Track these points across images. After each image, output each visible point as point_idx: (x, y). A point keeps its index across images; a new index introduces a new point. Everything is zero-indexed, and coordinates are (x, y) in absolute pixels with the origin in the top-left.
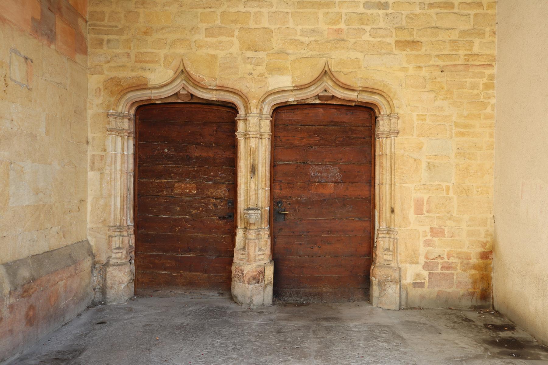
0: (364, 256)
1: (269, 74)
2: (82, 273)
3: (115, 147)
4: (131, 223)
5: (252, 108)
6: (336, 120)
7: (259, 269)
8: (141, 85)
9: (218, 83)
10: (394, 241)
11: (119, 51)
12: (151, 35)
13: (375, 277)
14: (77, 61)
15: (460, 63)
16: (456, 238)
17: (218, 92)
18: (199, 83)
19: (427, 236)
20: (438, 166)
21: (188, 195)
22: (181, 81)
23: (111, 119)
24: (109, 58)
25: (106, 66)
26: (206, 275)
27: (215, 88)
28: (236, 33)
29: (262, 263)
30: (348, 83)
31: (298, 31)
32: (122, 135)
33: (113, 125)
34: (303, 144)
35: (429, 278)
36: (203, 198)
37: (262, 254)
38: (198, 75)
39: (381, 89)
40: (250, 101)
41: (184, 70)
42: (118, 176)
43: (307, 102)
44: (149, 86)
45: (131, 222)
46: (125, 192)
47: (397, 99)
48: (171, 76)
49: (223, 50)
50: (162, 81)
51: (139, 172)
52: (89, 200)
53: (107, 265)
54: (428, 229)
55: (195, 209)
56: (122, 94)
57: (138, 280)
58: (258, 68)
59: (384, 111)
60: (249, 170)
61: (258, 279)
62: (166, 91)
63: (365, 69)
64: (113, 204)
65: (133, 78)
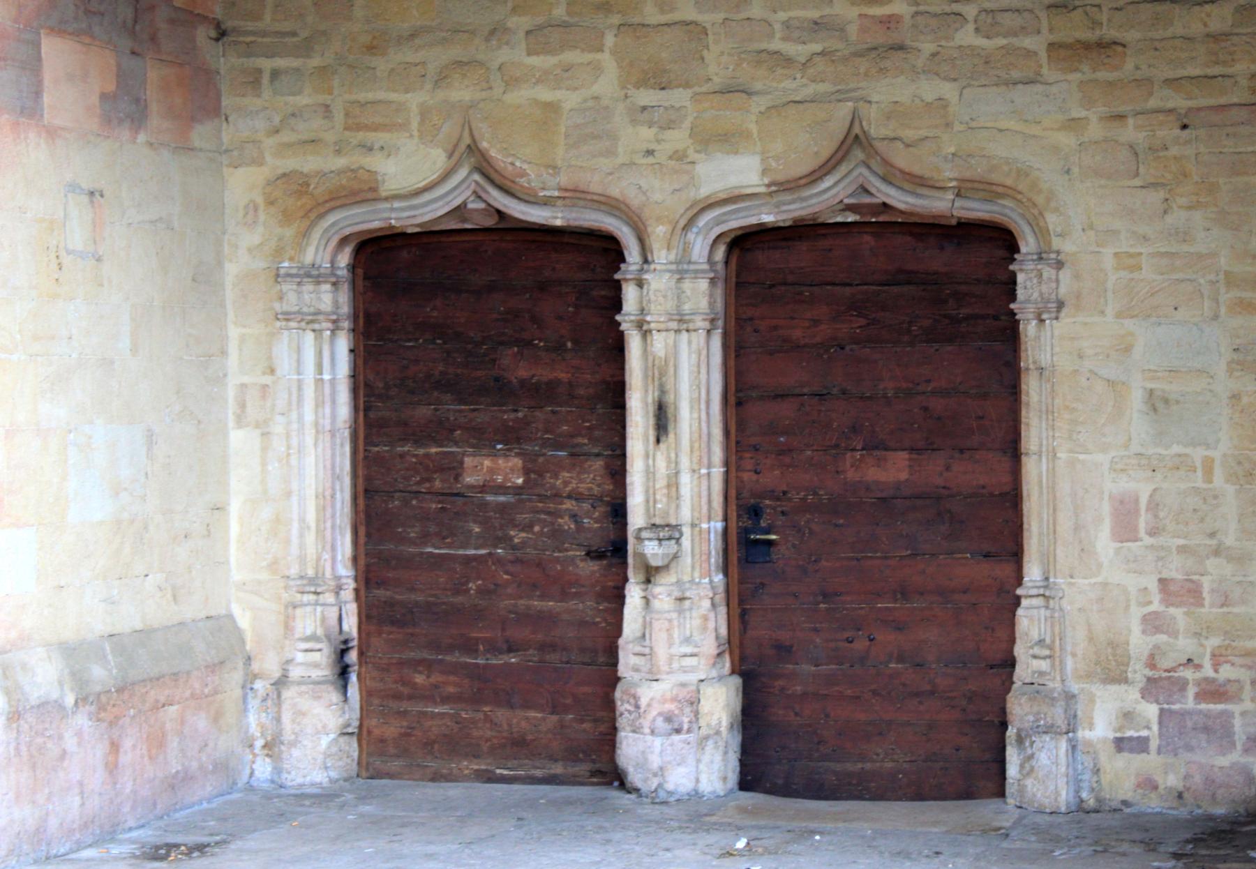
2: (219, 697)
3: (298, 361)
4: (346, 571)
8: (362, 191)
9: (563, 179)
11: (303, 100)
12: (383, 55)
15: (1235, 100)
16: (1236, 610)
19: (1150, 603)
20: (1178, 402)
21: (501, 489)
22: (470, 173)
23: (285, 287)
24: (277, 120)
26: (555, 718)
28: (610, 40)
29: (693, 678)
31: (777, 27)
32: (316, 326)
33: (292, 301)
34: (818, 339)
35: (1160, 723)
36: (542, 498)
38: (510, 160)
39: (1009, 182)
40: (649, 229)
42: (309, 440)
44: (384, 194)
45: (345, 566)
46: (328, 485)
47: (1057, 210)
49: (576, 89)
51: (369, 424)
52: (235, 507)
55: (523, 530)
56: (313, 216)
57: (369, 732)
58: (669, 134)
59: (1028, 245)
63: (962, 127)
64: (295, 517)
65: (340, 172)
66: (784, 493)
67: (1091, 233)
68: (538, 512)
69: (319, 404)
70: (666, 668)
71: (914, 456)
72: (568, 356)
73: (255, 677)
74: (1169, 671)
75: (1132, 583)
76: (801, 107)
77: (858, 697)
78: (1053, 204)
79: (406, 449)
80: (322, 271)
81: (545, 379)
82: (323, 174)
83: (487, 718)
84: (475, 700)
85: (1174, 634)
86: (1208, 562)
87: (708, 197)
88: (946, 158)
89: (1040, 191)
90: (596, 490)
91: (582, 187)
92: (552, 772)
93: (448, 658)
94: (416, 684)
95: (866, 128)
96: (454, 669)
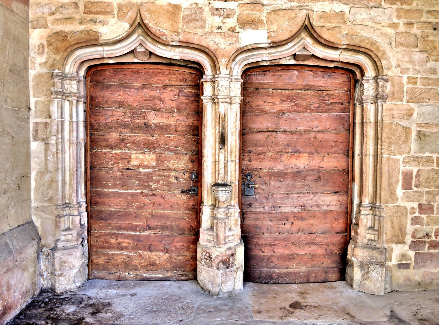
0: (339, 233)
1: (241, 28)
5: (221, 67)
6: (311, 83)
7: (229, 252)
9: (182, 38)
10: (379, 220)
13: (356, 258)
14: (15, 10)
17: (181, 50)
18: (159, 38)
19: (415, 213)
20: (429, 136)
21: (147, 167)
23: (56, 80)
24: (54, 9)
25: (50, 19)
26: (168, 255)
27: (178, 44)
29: (232, 245)
30: (332, 40)
32: (70, 99)
35: (415, 258)
37: (233, 235)
38: (158, 28)
39: (368, 47)
40: (219, 60)
41: (141, 23)
43: (280, 63)
44: (101, 42)
46: (75, 165)
47: (386, 59)
48: (126, 29)
50: (116, 36)
52: (33, 175)
53: (54, 249)
54: (416, 205)
55: (155, 183)
58: (227, 20)
60: (218, 140)
61: (227, 263)
62: (120, 48)
65: (81, 32)
66: (260, 169)
67: (399, 69)
68: (161, 176)
69: (71, 131)
70: (223, 242)
71: (311, 155)
72: (175, 115)
73: (43, 246)
74: (419, 238)
75: (409, 205)
76: (285, 11)
77: (286, 245)
78: (385, 57)
79: (107, 151)
80: (73, 75)
81: (165, 124)
82: (73, 33)
83: (140, 255)
84: (136, 248)
85: (422, 224)
86: (436, 197)
87: (243, 47)
88: (343, 35)
89: (380, 51)
90: (185, 168)
91: (190, 41)
92: (167, 275)
93: (124, 232)
94: (111, 243)
95: (311, 22)
96: (127, 237)
